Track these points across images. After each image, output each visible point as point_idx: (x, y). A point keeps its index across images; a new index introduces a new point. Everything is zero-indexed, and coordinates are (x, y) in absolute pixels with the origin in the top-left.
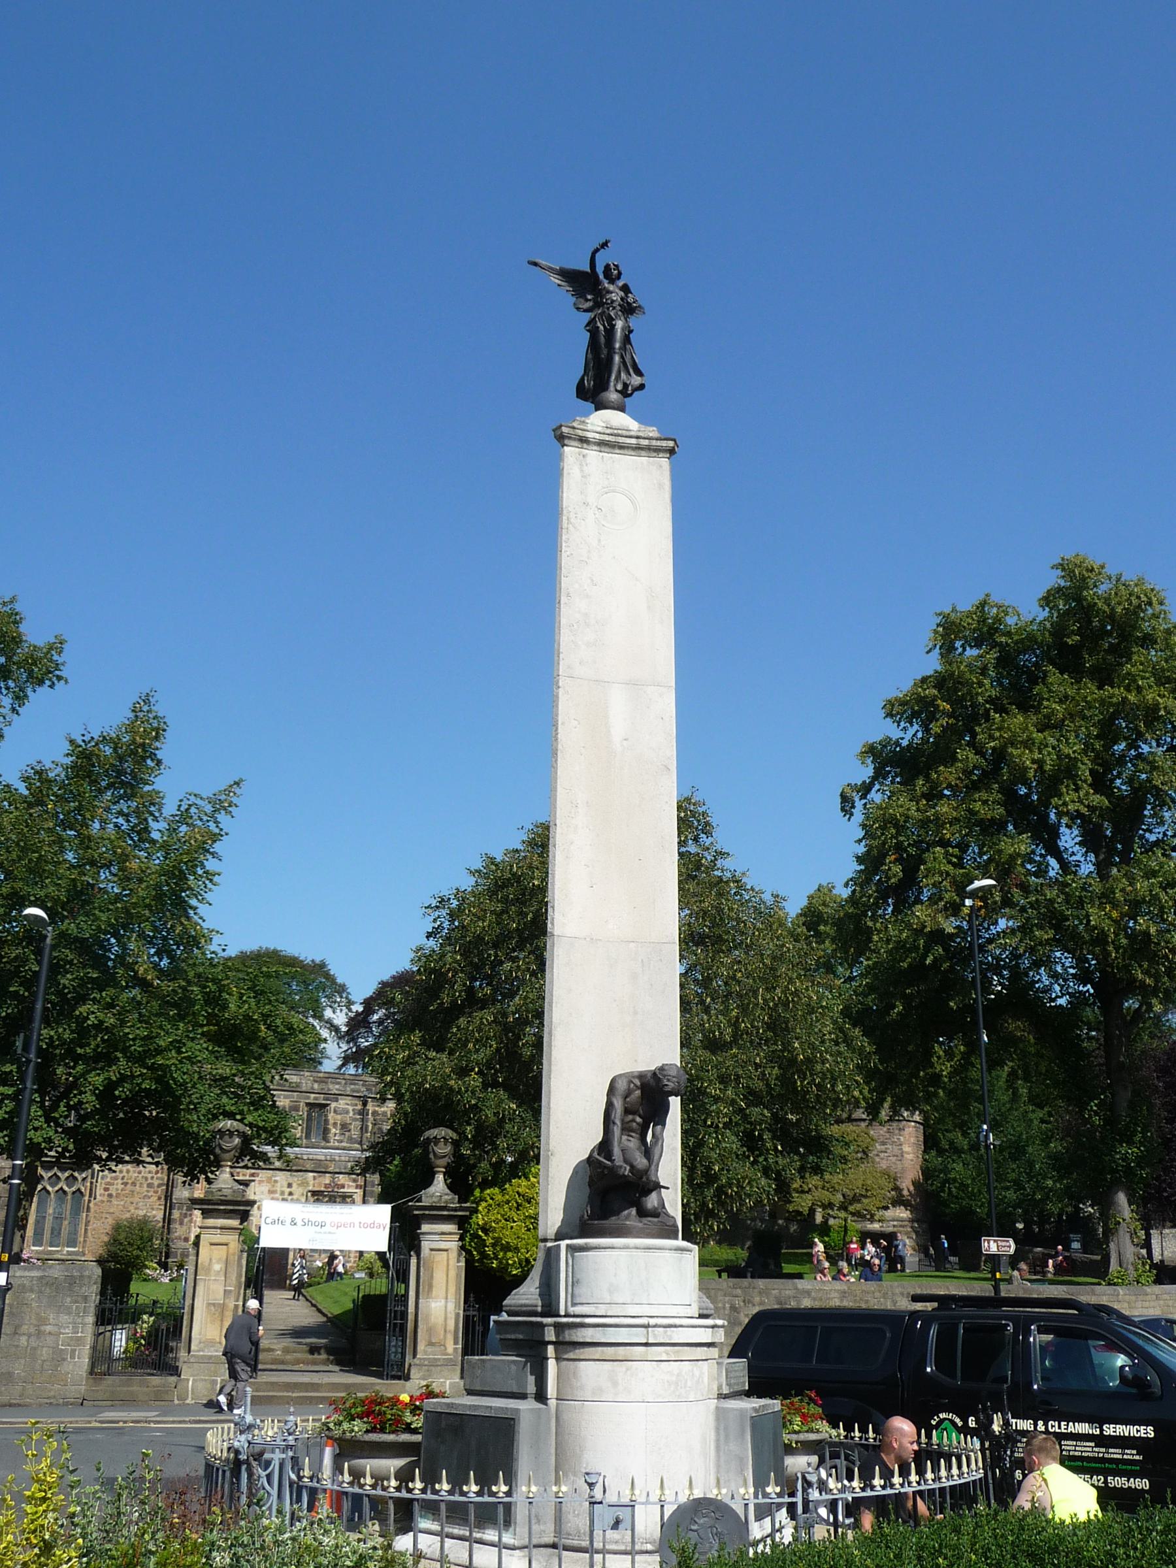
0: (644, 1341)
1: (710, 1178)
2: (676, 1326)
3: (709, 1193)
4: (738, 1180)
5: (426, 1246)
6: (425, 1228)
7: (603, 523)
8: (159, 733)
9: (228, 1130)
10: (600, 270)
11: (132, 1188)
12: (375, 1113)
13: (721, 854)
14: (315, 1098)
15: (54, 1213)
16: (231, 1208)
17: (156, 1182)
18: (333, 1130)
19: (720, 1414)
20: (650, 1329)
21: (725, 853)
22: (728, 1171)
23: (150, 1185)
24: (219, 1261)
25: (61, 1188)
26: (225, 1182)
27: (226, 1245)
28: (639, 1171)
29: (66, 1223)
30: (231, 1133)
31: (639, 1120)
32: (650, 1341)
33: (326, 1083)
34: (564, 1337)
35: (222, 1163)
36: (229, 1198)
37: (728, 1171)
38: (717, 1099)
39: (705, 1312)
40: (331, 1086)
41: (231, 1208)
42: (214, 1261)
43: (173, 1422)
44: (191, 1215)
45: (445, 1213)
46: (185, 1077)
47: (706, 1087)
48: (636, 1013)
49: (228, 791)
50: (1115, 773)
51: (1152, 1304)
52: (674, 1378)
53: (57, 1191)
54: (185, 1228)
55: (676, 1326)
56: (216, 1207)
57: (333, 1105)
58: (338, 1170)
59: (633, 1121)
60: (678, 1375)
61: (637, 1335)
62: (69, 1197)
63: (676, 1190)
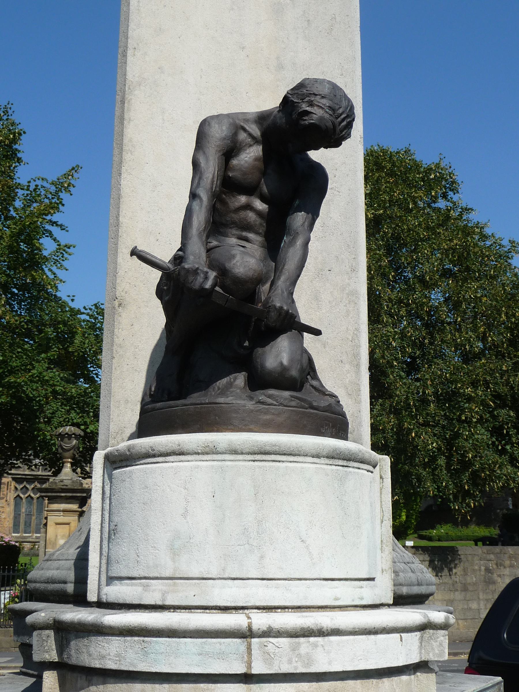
0: (239, 669)
1: (465, 465)
2: (321, 633)
3: (465, 477)
4: (489, 465)
8: (16, 137)
9: (67, 434)
13: (468, 210)
15: (26, 511)
16: (70, 495)
20: (254, 641)
21: (469, 209)
22: (481, 457)
24: (63, 537)
25: (30, 496)
26: (66, 475)
27: (68, 524)
28: (238, 281)
29: (34, 518)
30: (69, 436)
31: (260, 205)
32: (258, 669)
34: (69, 656)
35: (64, 460)
36: (69, 487)
37: (481, 457)
38: (470, 399)
41: (70, 495)
42: (59, 537)
46: (34, 393)
47: (460, 388)
48: (280, 67)
49: (66, 176)
53: (27, 497)
55: (321, 633)
56: (58, 494)
59: (248, 207)
61: (221, 656)
62: (35, 501)
63: (358, 366)
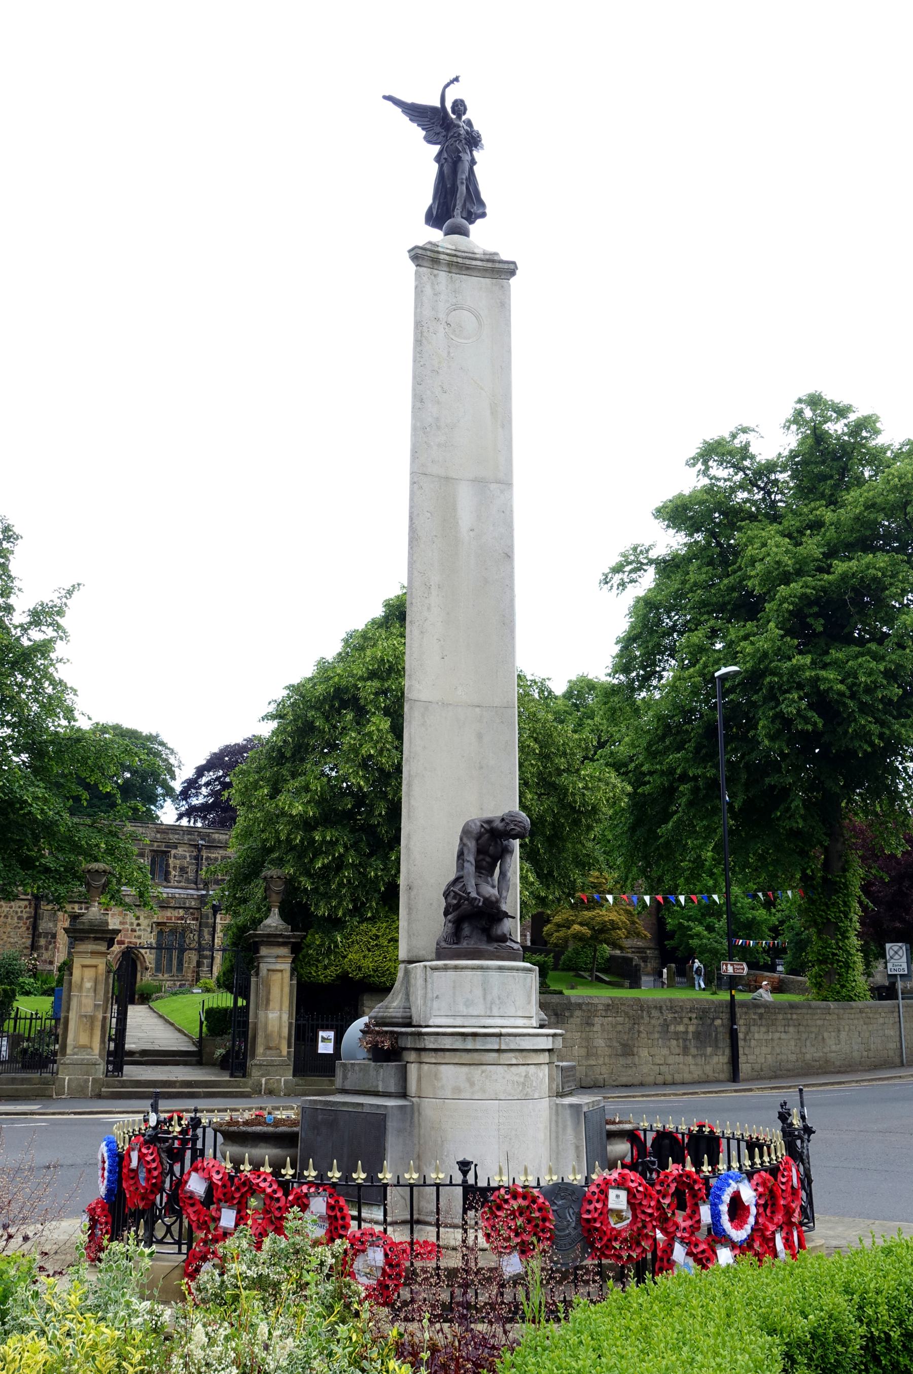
0: (497, 1047)
5: (263, 967)
6: (264, 951)
7: (453, 337)
10: (449, 106)
11: (5, 920)
12: (208, 858)
14: (158, 846)
17: (25, 916)
18: (173, 873)
19: (557, 1110)
23: (19, 918)
33: (167, 833)
39: (542, 1023)
40: (171, 836)
42: (85, 980)
43: (54, 1114)
44: (55, 942)
45: (281, 940)
50: (735, 595)
51: (857, 1016)
52: (522, 1080)
54: (50, 953)
57: (173, 852)
58: (177, 905)
59: (484, 860)
60: (526, 1076)
